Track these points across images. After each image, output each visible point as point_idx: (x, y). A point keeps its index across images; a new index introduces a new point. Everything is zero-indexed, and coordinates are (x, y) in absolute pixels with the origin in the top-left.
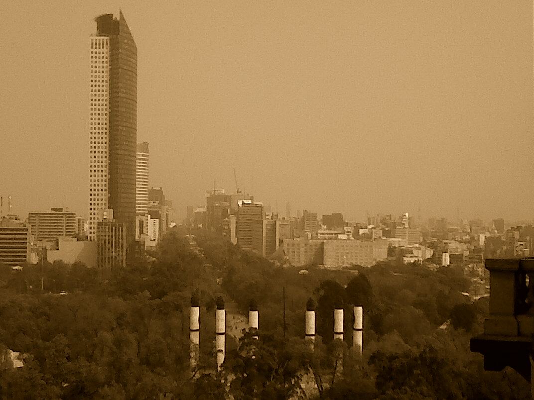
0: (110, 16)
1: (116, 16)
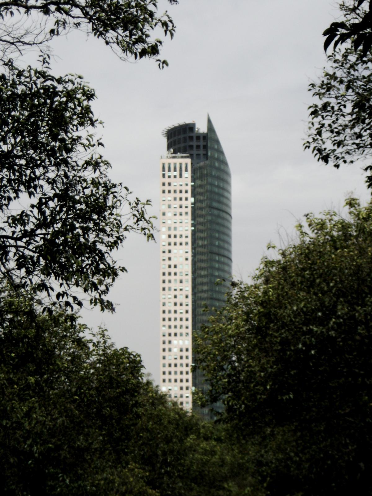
0: (188, 128)
1: (202, 128)
